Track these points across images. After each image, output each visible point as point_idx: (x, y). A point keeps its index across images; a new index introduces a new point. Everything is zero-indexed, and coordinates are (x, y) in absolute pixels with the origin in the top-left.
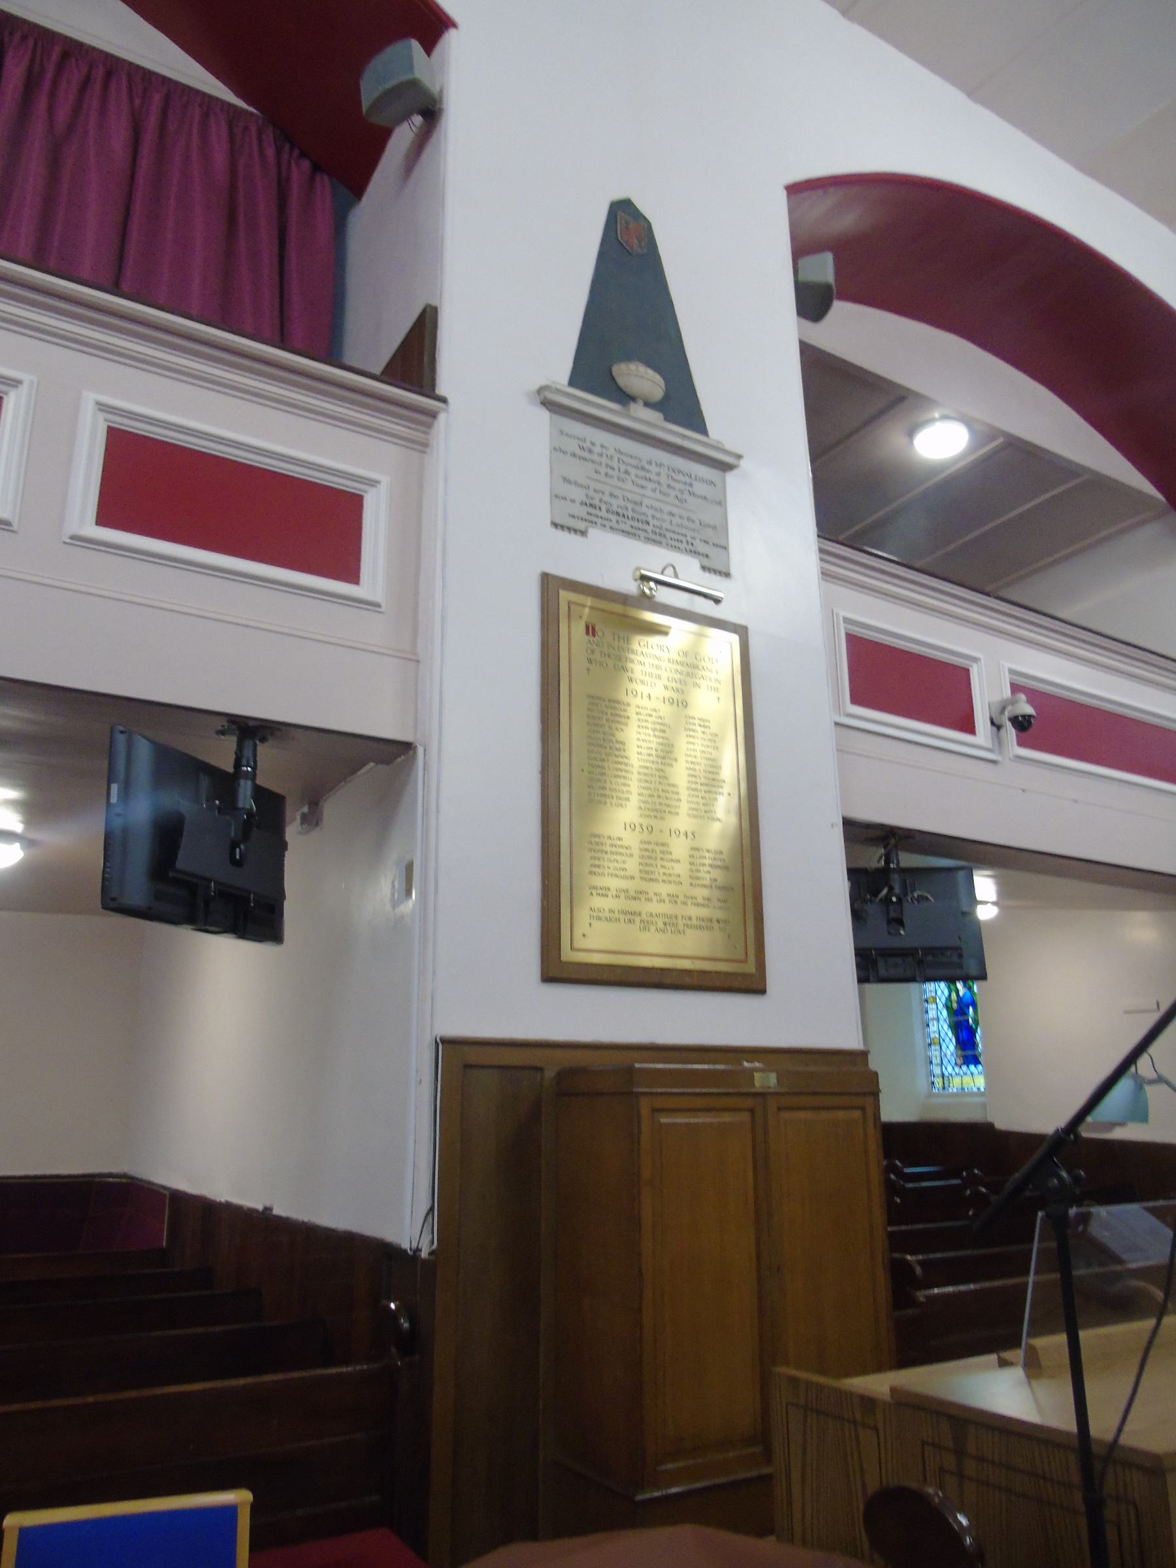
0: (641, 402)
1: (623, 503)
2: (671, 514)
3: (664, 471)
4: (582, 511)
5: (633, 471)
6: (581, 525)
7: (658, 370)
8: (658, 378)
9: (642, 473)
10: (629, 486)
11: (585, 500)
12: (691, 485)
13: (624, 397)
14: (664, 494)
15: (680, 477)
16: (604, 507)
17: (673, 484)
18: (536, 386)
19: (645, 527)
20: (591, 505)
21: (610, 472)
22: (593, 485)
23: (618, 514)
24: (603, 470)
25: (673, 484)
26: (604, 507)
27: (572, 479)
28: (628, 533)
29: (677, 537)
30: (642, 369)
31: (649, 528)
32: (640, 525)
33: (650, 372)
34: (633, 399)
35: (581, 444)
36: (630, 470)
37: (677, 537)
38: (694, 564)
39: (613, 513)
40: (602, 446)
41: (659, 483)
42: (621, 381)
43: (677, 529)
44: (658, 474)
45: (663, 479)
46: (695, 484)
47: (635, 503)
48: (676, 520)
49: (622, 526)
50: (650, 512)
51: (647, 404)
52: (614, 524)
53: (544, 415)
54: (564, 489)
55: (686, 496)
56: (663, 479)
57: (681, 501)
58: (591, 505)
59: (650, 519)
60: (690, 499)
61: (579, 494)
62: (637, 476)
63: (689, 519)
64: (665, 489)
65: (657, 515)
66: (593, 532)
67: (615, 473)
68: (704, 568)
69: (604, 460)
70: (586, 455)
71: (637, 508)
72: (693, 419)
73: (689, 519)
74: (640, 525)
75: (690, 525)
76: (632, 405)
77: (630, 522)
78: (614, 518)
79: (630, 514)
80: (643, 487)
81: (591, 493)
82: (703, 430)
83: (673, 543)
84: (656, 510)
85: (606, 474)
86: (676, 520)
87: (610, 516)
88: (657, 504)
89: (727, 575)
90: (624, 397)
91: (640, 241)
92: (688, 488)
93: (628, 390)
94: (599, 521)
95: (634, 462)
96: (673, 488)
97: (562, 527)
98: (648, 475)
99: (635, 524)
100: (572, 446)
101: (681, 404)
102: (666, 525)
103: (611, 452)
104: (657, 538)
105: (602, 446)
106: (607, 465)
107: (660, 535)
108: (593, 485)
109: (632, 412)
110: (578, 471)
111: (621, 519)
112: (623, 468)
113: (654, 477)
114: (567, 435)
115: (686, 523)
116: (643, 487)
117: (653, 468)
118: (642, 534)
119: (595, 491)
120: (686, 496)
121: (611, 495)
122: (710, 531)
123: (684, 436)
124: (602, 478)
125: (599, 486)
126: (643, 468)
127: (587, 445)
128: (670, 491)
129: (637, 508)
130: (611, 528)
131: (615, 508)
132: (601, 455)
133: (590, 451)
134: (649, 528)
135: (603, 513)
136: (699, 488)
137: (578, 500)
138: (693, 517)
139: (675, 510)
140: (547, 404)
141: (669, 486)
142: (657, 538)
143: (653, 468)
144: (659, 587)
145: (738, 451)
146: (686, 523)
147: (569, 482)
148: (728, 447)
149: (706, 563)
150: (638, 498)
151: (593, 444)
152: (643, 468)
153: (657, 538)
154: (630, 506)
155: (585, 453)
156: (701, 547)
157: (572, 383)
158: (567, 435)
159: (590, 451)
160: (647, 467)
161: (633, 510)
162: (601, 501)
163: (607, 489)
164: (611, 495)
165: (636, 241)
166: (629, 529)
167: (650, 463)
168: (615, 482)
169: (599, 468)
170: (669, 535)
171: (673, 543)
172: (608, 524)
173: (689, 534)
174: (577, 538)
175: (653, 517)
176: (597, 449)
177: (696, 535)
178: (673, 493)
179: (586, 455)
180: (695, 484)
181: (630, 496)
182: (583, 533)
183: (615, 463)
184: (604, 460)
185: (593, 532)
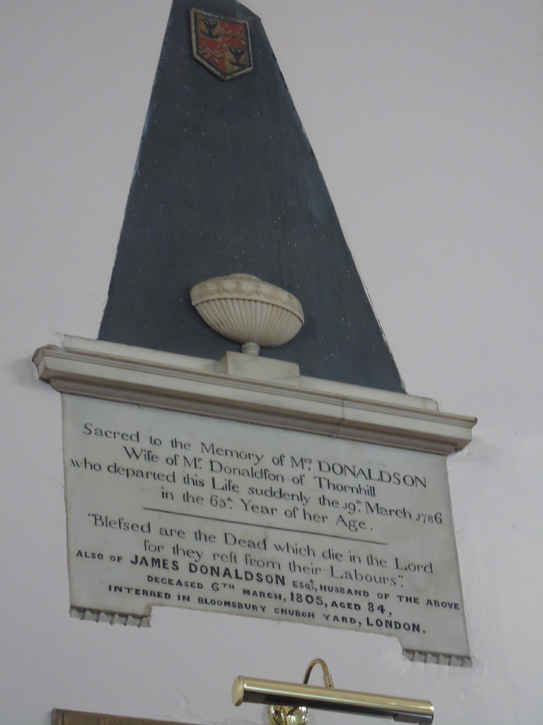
0: (253, 348)
1: (225, 549)
2: (332, 555)
3: (311, 473)
4: (138, 576)
5: (244, 483)
6: (137, 605)
7: (289, 288)
8: (283, 296)
9: (264, 484)
10: (236, 512)
11: (141, 553)
12: (372, 491)
13: (217, 343)
14: (313, 517)
15: (348, 480)
16: (184, 562)
17: (331, 495)
18: (32, 352)
19: (277, 588)
20: (156, 561)
21: (194, 491)
22: (159, 522)
23: (215, 571)
24: (178, 488)
25: (331, 495)
26: (184, 562)
27: (113, 517)
28: (240, 606)
29: (346, 598)
30: (249, 285)
31: (285, 591)
32: (265, 587)
33: (266, 288)
34: (238, 344)
35: (130, 444)
36: (236, 479)
37: (346, 598)
38: (388, 649)
39: (204, 570)
40: (174, 443)
41: (301, 497)
42: (211, 314)
43: (347, 584)
44: (300, 481)
45: (310, 488)
46: (379, 486)
47: (252, 544)
48: (343, 566)
49: (224, 594)
50: (285, 558)
51: (267, 350)
52: (207, 593)
53: (51, 399)
54: (94, 538)
55: (362, 514)
56: (310, 488)
57: (349, 525)
58: (156, 561)
59: (284, 571)
60: (373, 520)
61: (130, 544)
62: (252, 491)
63: (370, 560)
64: (314, 507)
65: (302, 560)
66: (160, 614)
67: (206, 492)
68: (410, 653)
69: (180, 469)
70: (142, 464)
71: (255, 553)
72: (374, 364)
73: (370, 560)
74: (265, 587)
75: (375, 570)
76: (232, 356)
77: (243, 584)
78: (207, 580)
79: (242, 567)
80: (266, 510)
81: (155, 538)
82: (392, 381)
83: (340, 612)
84: (296, 551)
85: (186, 497)
86: (343, 566)
87: (198, 577)
88: (300, 541)
89: (464, 660)
90: (217, 343)
91: (237, 55)
92: (364, 498)
93: (226, 329)
94: (174, 590)
95: (246, 464)
96: (333, 503)
97: (96, 612)
98: (276, 486)
99: (253, 586)
100: (111, 451)
101: (344, 338)
102: (321, 579)
103: (194, 452)
104: (304, 606)
105: (174, 443)
106: (186, 479)
107: (309, 599)
108: (159, 522)
109: (232, 372)
110: (125, 498)
111: (220, 580)
112: (221, 479)
113: (289, 488)
114: (101, 433)
115: (363, 568)
116: (266, 510)
117: (288, 471)
118: (271, 604)
119: (164, 532)
120: (362, 514)
121: (198, 535)
122: (420, 577)
123: (344, 400)
124: (178, 504)
125: (170, 522)
126: (264, 473)
127: (145, 444)
128: (326, 510)
129: (255, 553)
130: (200, 600)
131: (208, 561)
132: (174, 461)
133: (150, 457)
134: (285, 591)
135: (183, 574)
136: (388, 495)
137: (128, 557)
138: (378, 552)
139: (338, 546)
140: (49, 379)
141: (323, 500)
142: (303, 607)
143: (288, 471)
144: (312, 711)
145: (470, 414)
146: (363, 568)
147: (107, 523)
148: (445, 408)
149: (414, 640)
150: (257, 535)
151: (154, 441)
152: (264, 473)
153: (303, 607)
154: (240, 551)
155: (138, 462)
156: (399, 612)
157: (107, 333)
158: (101, 433)
159: (150, 457)
160: (274, 469)
161: (248, 559)
162: (176, 550)
163: (190, 526)
164: (198, 535)
165: (229, 56)
166: (236, 596)
167: (280, 461)
168: (206, 509)
169: (169, 487)
170: (328, 597)
171: (340, 612)
172: (194, 593)
173: (374, 588)
174: (131, 630)
175: (292, 566)
176: (165, 451)
177: (383, 588)
178: (333, 513)
179: (142, 464)
180: (379, 486)
181: (239, 532)
182: (142, 619)
183: (204, 474)
184: (180, 469)
185: (160, 614)
